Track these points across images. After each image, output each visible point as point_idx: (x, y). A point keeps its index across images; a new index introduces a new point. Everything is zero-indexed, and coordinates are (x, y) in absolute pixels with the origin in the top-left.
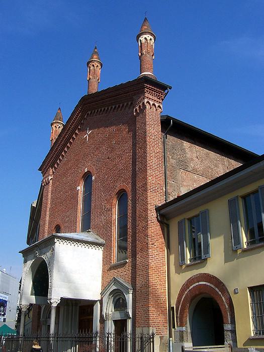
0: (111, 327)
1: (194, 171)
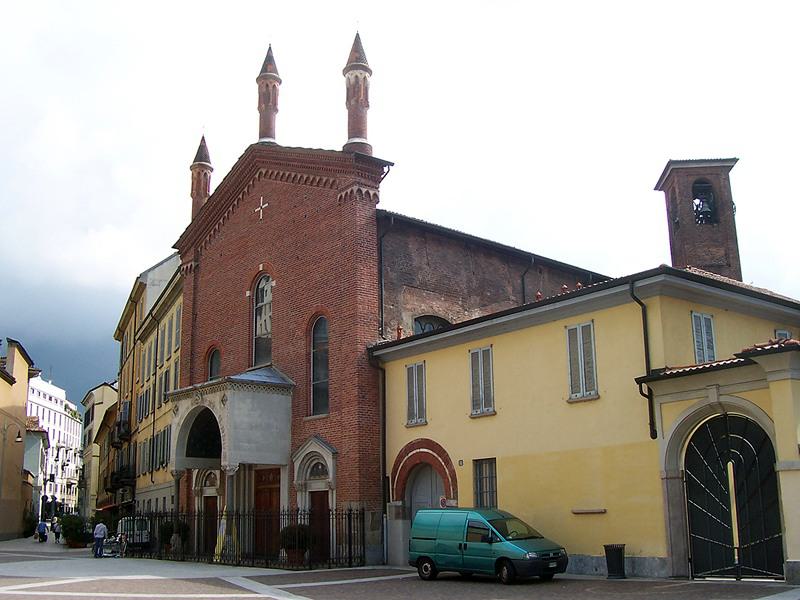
0: (303, 502)
1: (424, 286)
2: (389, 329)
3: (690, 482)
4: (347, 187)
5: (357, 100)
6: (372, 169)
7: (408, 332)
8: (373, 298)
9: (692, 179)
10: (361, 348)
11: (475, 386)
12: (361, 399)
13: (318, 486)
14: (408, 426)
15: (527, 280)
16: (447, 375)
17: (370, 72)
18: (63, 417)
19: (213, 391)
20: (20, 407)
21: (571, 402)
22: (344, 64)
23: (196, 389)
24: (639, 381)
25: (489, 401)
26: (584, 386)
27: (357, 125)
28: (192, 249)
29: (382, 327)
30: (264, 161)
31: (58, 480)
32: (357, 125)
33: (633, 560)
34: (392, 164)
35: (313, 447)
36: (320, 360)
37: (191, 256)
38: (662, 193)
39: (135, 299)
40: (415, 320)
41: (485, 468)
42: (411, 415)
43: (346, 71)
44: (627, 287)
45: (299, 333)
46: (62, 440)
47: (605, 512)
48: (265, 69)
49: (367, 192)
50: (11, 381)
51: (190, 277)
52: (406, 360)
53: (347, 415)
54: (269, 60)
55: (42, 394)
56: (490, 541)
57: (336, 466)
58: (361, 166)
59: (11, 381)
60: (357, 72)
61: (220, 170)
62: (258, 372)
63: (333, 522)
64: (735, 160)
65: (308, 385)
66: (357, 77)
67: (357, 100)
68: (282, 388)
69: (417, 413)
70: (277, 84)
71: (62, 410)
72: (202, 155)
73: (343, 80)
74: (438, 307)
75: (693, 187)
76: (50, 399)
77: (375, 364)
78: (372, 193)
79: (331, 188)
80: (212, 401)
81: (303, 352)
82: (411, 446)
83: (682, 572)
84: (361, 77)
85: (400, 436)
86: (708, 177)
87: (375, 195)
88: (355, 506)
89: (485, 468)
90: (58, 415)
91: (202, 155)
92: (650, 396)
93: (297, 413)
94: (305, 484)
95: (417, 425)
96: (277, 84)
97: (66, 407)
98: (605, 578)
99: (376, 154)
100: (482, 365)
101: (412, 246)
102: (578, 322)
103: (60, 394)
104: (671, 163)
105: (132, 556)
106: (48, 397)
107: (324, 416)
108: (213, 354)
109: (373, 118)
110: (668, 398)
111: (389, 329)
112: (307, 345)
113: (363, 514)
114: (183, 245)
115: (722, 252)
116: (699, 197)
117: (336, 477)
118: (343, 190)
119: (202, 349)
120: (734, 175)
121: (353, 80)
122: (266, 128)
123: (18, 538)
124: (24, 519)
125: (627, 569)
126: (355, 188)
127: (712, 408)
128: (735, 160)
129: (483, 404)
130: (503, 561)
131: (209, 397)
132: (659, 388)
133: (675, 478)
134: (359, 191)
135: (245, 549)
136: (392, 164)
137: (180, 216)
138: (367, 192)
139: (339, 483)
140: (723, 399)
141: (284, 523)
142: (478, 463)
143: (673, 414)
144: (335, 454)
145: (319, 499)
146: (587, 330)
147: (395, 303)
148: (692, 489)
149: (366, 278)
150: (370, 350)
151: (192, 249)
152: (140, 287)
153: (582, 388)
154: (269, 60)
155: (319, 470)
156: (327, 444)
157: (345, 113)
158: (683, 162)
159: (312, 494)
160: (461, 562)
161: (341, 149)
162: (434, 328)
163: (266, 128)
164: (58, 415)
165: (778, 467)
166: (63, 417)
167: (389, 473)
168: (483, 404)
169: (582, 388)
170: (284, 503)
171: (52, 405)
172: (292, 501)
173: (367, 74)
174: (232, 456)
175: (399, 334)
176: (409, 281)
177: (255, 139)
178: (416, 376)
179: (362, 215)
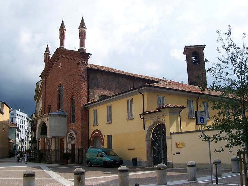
0: (70, 147)
2: (91, 100)
3: (153, 141)
4: (79, 61)
5: (82, 36)
6: (87, 56)
7: (97, 100)
8: (86, 91)
9: (192, 51)
10: (82, 105)
11: (108, 116)
12: (82, 119)
13: (73, 142)
14: (94, 126)
15: (134, 84)
16: (102, 111)
17: (86, 29)
18: (27, 122)
19: (45, 117)
20: (7, 121)
21: (128, 120)
22: (79, 27)
23: (41, 116)
24: (140, 115)
25: (110, 119)
26: (130, 116)
27: (82, 44)
28: (45, 77)
29: (88, 99)
30: (61, 52)
31: (25, 141)
32: (82, 44)
33: (140, 162)
34: (91, 54)
35: (71, 132)
36: (73, 109)
37: (44, 79)
38: (185, 55)
39: (37, 90)
40: (99, 97)
41: (110, 137)
42: (94, 124)
43: (79, 28)
44: (138, 90)
45: (69, 101)
46: (27, 129)
47: (134, 149)
48: (61, 27)
49: (84, 62)
50: (3, 114)
51: (44, 85)
52: (93, 108)
53: (78, 124)
54: (63, 24)
55: (20, 116)
56: (102, 157)
57: (76, 138)
58: (83, 55)
59: (3, 114)
60: (82, 29)
61: (52, 53)
62: (58, 112)
63: (76, 152)
64: (205, 45)
65: (71, 115)
66: (82, 30)
67: (82, 36)
68: (64, 116)
69: (96, 123)
70: (65, 31)
71: (27, 120)
72: (47, 50)
73: (78, 30)
74: (106, 93)
75: (193, 54)
76: (23, 117)
77: (86, 110)
78: (85, 62)
79: (76, 61)
80: (45, 119)
81: (69, 106)
82: (94, 131)
83: (150, 165)
84: (83, 30)
85: (92, 129)
86: (197, 51)
87: (87, 63)
88: (80, 147)
89: (110, 137)
90: (25, 122)
91: (47, 50)
92: (144, 119)
93: (69, 122)
94: (70, 142)
95: (95, 126)
96: (65, 31)
97: (28, 119)
98: (132, 166)
99: (87, 52)
100: (109, 109)
101: (98, 76)
102: (129, 98)
103: (26, 115)
104: (186, 47)
105: (30, 162)
106: (22, 116)
107: (74, 123)
108: (50, 106)
109: (86, 41)
110: (147, 119)
111: (91, 100)
112: (71, 104)
113: (82, 150)
114: (44, 75)
115: (201, 73)
116: (195, 55)
117: (76, 140)
118: (77, 62)
119: (47, 105)
120: (205, 52)
121: (81, 31)
122: (62, 43)
123: (8, 158)
124: (9, 152)
125: (138, 164)
126: (81, 61)
127: (157, 122)
128: (205, 45)
129: (109, 120)
130: (105, 162)
131: (44, 119)
132: (146, 116)
133: (149, 140)
134: (82, 62)
135: (57, 159)
136: (91, 54)
137: (41, 68)
138: (84, 62)
139: (77, 142)
140: (159, 120)
141: (65, 152)
142: (108, 136)
143: (148, 124)
144: (76, 134)
145: (73, 145)
146: (131, 100)
147: (93, 92)
148: (154, 144)
149: (84, 85)
150: (84, 106)
151: (45, 77)
152: (37, 86)
153: (130, 116)
154: (63, 24)
155: (73, 138)
156: (74, 131)
157: (79, 40)
158: (196, 46)
159: (71, 144)
160: (96, 162)
161: (77, 51)
162: (103, 98)
163: (62, 43)
164: (25, 122)
165: (166, 138)
166: (27, 122)
167: (90, 139)
168: (109, 120)
169: (130, 116)
170: (65, 147)
171: (23, 119)
172: (67, 147)
173: (85, 29)
174: (49, 135)
175: (93, 101)
176: (97, 86)
177: (58, 47)
178: (95, 112)
179: (83, 68)
